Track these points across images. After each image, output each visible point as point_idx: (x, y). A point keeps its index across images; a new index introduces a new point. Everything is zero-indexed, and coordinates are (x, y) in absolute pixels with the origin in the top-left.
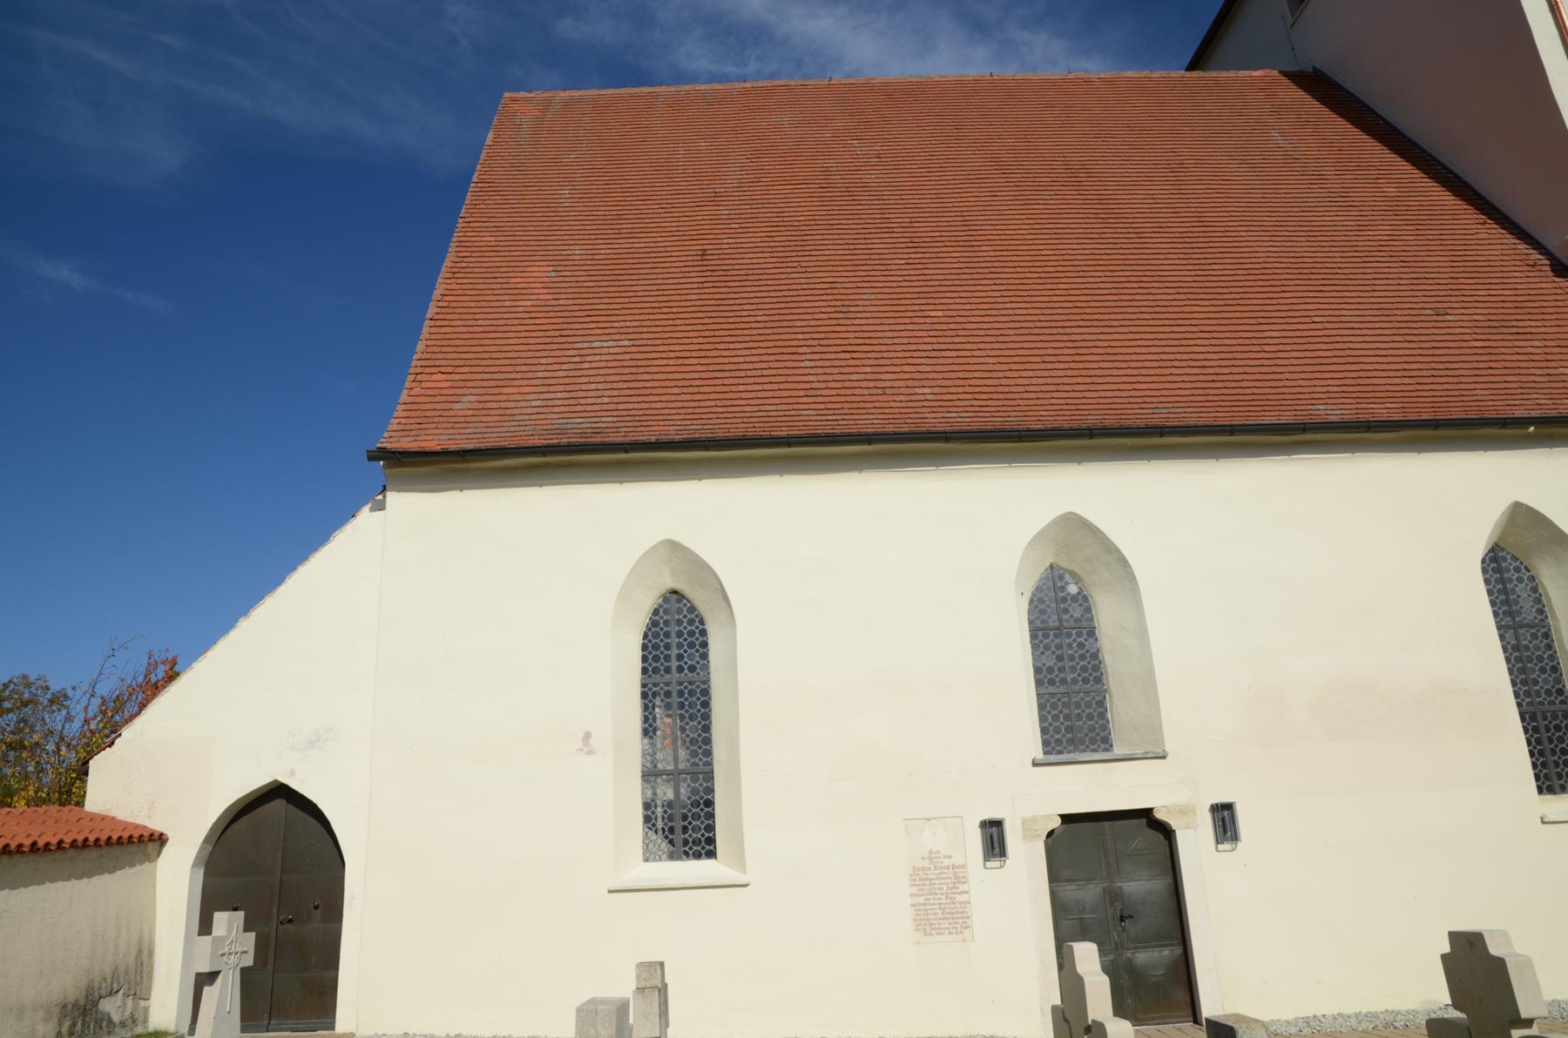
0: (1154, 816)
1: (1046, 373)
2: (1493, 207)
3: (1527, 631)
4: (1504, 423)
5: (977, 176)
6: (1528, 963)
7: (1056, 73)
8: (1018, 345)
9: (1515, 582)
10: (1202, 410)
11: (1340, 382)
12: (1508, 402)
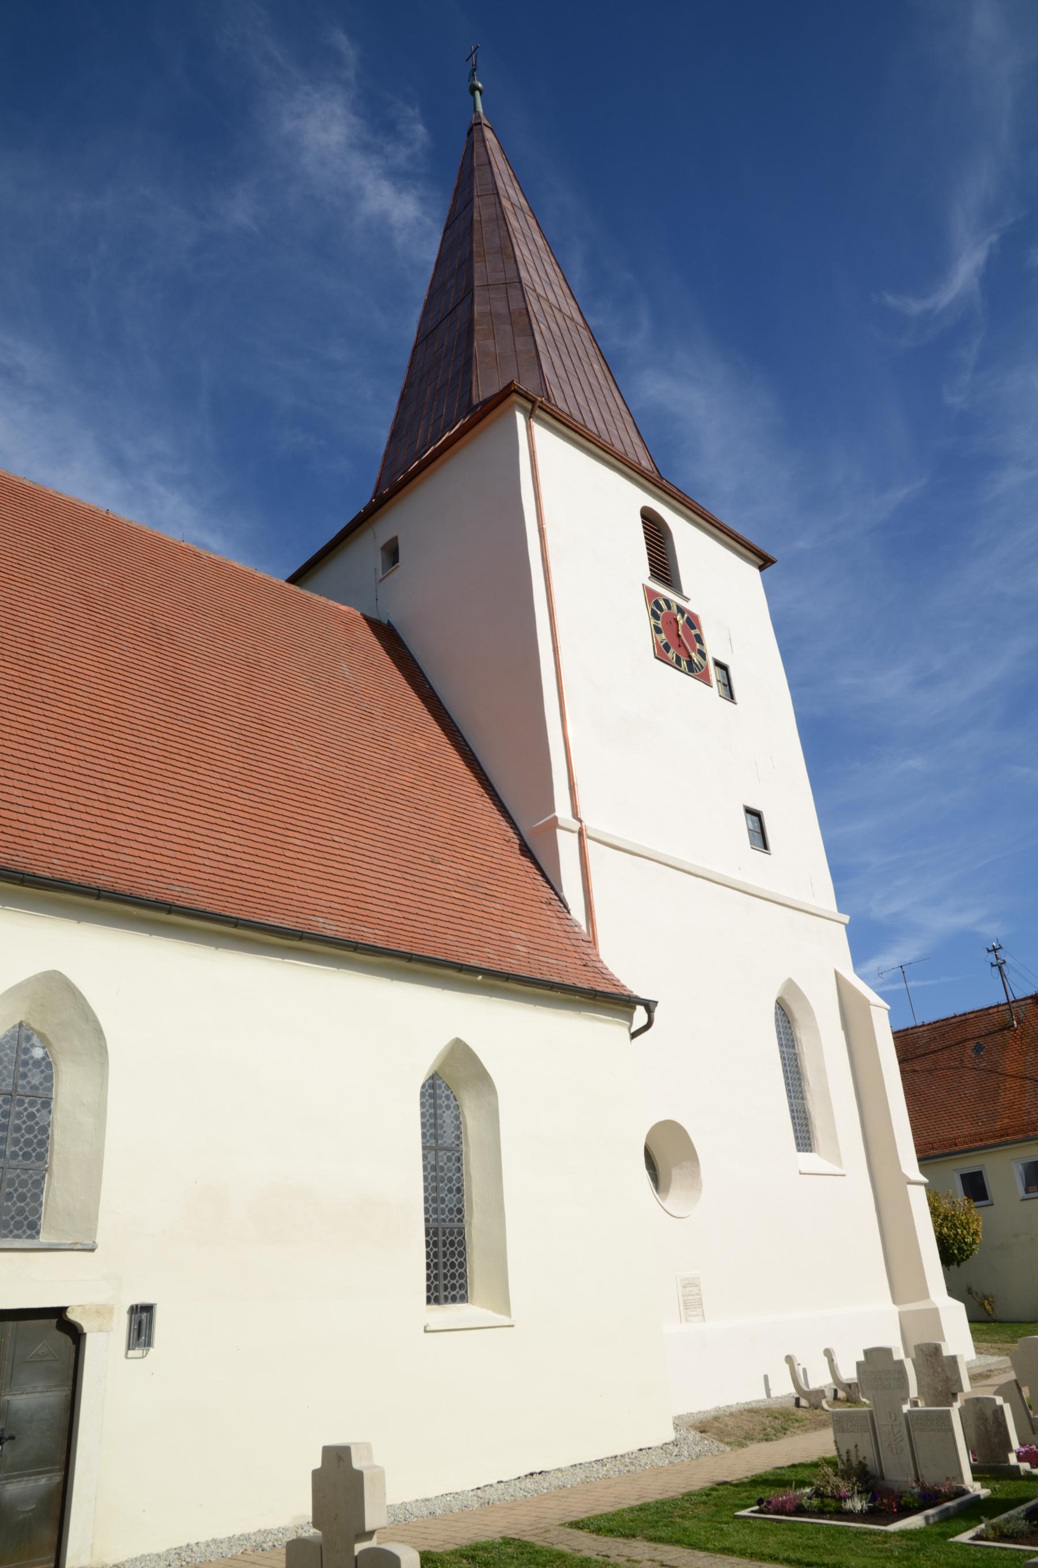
0: (66, 1316)
1: (71, 821)
2: (491, 785)
3: (445, 1154)
4: (461, 968)
5: (60, 603)
6: (381, 1474)
7: (172, 535)
8: (49, 784)
9: (444, 1109)
10: (215, 897)
11: (342, 901)
12: (468, 951)
